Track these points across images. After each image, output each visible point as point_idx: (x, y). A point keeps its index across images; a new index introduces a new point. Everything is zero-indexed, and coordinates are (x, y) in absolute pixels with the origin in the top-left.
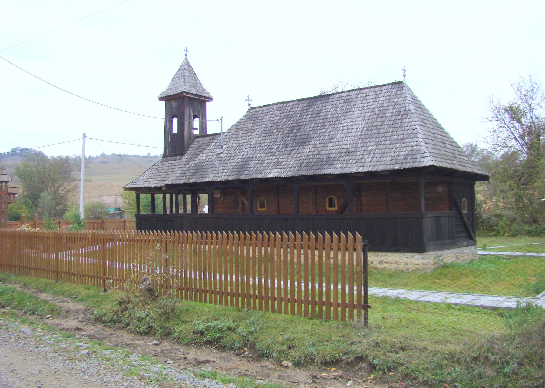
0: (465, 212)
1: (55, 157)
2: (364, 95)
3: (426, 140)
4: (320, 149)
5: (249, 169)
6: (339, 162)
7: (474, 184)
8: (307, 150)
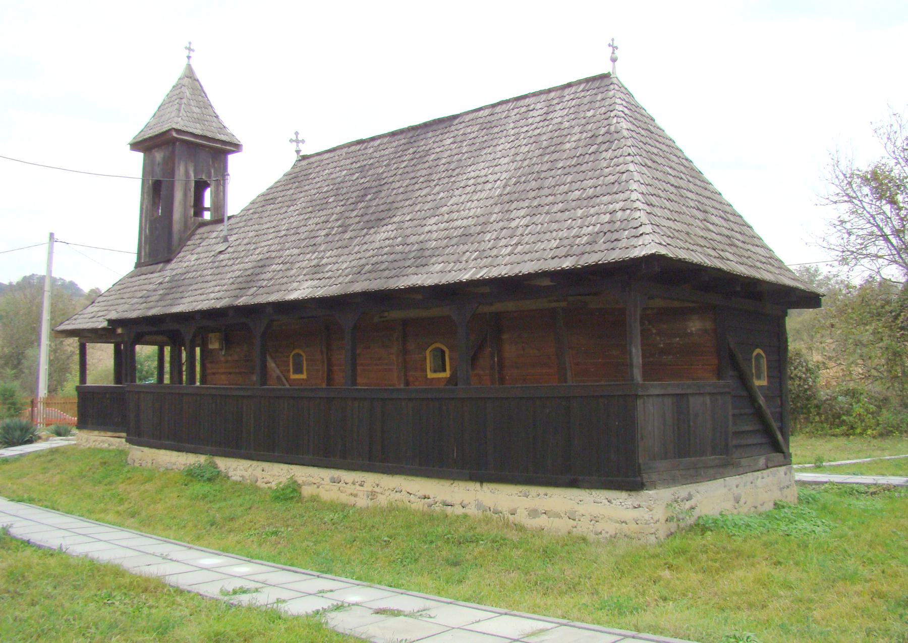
0: (760, 382)
1: (15, 283)
2: (524, 109)
3: (653, 200)
5: (259, 284)
8: (382, 235)
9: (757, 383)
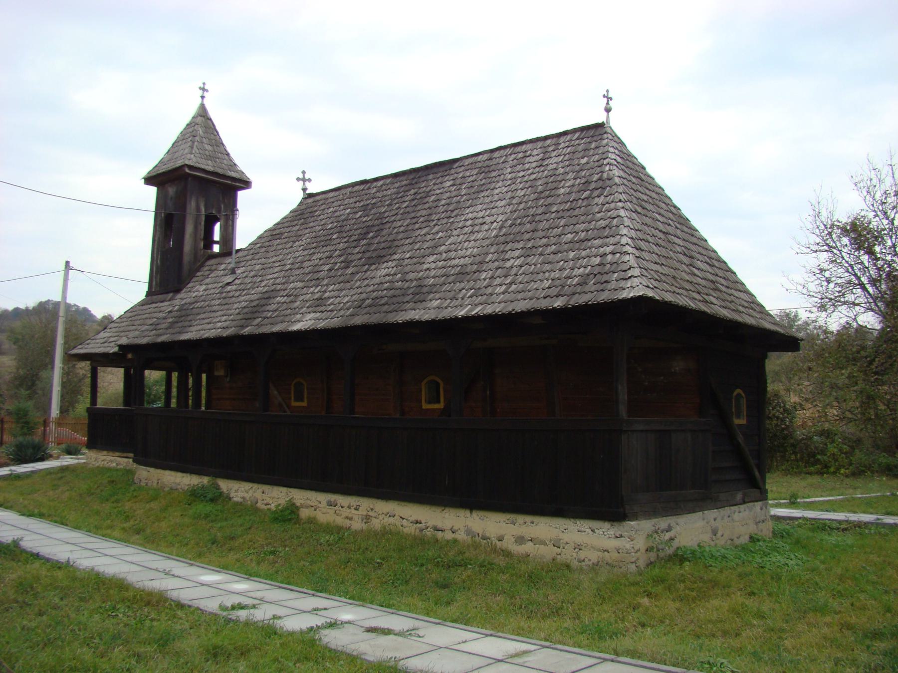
2: (520, 155)
3: (642, 244)
4: (407, 269)
6: (438, 296)
7: (765, 357)
8: (383, 271)
9: (737, 421)
